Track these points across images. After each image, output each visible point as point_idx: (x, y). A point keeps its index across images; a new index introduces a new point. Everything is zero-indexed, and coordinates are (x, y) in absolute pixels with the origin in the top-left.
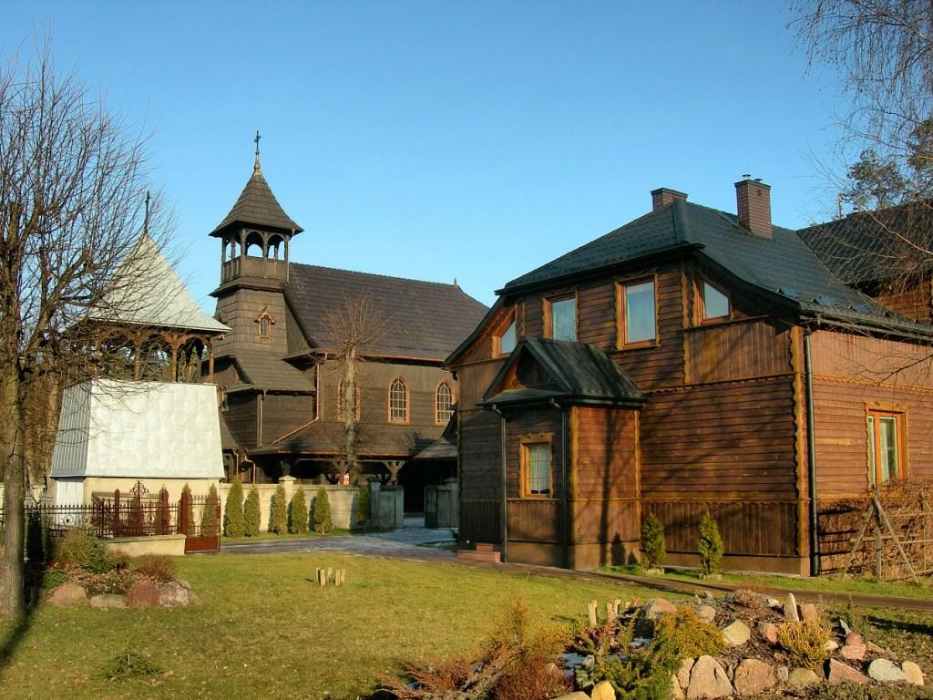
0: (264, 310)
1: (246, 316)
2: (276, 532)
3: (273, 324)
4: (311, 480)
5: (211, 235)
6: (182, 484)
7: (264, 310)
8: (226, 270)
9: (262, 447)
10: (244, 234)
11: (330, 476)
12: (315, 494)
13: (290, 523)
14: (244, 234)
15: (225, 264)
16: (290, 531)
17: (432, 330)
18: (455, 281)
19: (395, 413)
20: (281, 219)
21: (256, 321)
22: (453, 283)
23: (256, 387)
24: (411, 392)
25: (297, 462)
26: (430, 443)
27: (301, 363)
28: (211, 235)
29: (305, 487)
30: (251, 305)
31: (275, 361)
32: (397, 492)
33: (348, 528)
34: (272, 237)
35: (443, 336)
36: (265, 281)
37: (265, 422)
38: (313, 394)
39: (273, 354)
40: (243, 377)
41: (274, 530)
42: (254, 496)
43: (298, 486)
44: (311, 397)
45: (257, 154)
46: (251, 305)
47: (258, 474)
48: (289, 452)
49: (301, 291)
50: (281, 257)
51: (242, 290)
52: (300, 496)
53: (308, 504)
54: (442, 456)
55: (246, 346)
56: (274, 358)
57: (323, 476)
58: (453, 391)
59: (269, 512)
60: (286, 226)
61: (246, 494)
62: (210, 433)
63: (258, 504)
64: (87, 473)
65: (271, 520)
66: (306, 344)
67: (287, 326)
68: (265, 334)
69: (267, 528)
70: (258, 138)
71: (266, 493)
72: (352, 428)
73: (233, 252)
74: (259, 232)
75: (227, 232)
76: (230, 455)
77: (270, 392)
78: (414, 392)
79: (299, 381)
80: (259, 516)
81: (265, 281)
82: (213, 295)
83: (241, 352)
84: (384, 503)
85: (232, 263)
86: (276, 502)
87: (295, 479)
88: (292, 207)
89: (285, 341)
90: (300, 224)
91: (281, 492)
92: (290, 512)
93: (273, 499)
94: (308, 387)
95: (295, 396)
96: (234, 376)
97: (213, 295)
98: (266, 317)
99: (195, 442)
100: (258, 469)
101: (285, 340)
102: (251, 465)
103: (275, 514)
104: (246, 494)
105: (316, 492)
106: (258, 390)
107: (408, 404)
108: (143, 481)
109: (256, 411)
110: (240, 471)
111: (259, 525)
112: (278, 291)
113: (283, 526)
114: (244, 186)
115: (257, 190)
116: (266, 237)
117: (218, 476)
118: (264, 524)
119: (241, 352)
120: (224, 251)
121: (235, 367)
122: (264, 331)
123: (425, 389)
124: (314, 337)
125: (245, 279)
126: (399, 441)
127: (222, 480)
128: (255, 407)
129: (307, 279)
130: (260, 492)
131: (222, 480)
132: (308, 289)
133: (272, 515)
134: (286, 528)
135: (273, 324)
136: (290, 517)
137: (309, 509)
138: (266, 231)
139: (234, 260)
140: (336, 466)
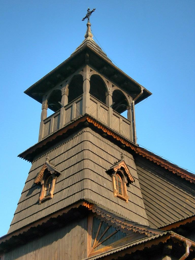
5: (21, 156)
21: (110, 172)
51: (88, 129)
90: (149, 89)
116: (111, 88)
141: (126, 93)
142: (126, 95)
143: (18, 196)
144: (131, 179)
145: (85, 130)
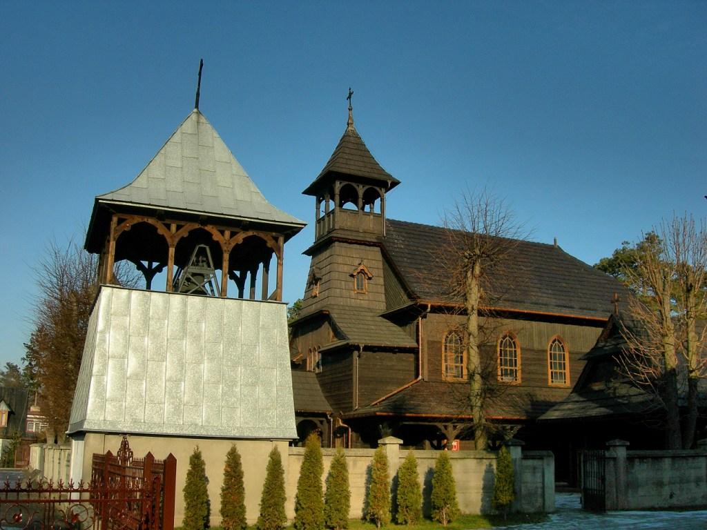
0: (360, 264)
1: (340, 270)
2: (374, 521)
3: (370, 279)
4: (414, 447)
5: (303, 193)
6: (228, 446)
7: (360, 264)
8: (320, 227)
9: (359, 406)
10: (338, 186)
11: (435, 443)
12: (433, 464)
13: (395, 509)
14: (338, 186)
15: (319, 221)
16: (394, 521)
17: (539, 286)
18: (555, 241)
19: (505, 373)
20: (376, 171)
21: (352, 276)
22: (552, 243)
23: (351, 342)
24: (521, 349)
25: (401, 424)
26: (550, 405)
27: (402, 317)
28: (303, 193)
29: (416, 453)
30: (347, 259)
31: (373, 316)
32: (545, 460)
33: (479, 513)
34: (367, 190)
35: (550, 291)
36: (361, 235)
37: (362, 381)
38: (414, 351)
39: (370, 310)
40: (338, 333)
41: (370, 518)
42: (340, 468)
43: (406, 452)
44: (412, 355)
45: (350, 110)
46: (345, 258)
47: (354, 439)
48: (391, 414)
49: (398, 244)
50: (377, 210)
51: (336, 243)
52: (410, 468)
53: (421, 479)
54: (576, 415)
55: (341, 301)
56: (371, 314)
57: (427, 442)
58: (566, 349)
59: (363, 491)
60: (382, 178)
61: (327, 464)
62: (276, 372)
63: (345, 480)
64: (86, 427)
65: (367, 504)
66: (405, 297)
67: (384, 281)
68: (362, 289)
69: (360, 514)
70: (351, 94)
71: (358, 462)
72: (479, 370)
73: (327, 206)
74: (354, 185)
75: (319, 189)
76: (324, 419)
77: (367, 348)
78: (527, 350)
79: (398, 336)
80: (347, 498)
81: (361, 235)
82: (308, 253)
83: (335, 307)
84: (528, 477)
85: (326, 219)
86: (373, 477)
87: (401, 442)
88: (388, 164)
89: (383, 297)
90: (396, 176)
91: (382, 461)
92: (394, 490)
93: (370, 471)
94: (409, 343)
95: (395, 353)
96: (329, 334)
97: (308, 253)
98: (362, 272)
99: (254, 385)
100: (354, 434)
101: (383, 296)
102: (347, 429)
103: (372, 493)
104: (327, 464)
105: (372, 458)
106: (354, 346)
107: (519, 362)
108: (239, 444)
109: (351, 370)
110: (335, 436)
111: (347, 511)
112: (374, 245)
113: (385, 513)
114: (338, 142)
115: (351, 144)
116: (361, 190)
117: (287, 436)
118: (356, 507)
119: (335, 307)
120: (318, 208)
121: (330, 323)
122: (360, 286)
123: (536, 346)
124: (416, 288)
125: (339, 232)
126: (514, 405)
127: (293, 443)
128: (350, 367)
129: (404, 234)
130: (350, 462)
131: (293, 443)
132: (406, 243)
133: (367, 495)
134: (389, 516)
135: (370, 279)
136: (395, 499)
137: (422, 487)
138: (361, 183)
139: (328, 214)
140: (444, 431)
141: (378, 186)
142: (378, 189)
143: (305, 286)
144: (370, 276)
145: (333, 244)
